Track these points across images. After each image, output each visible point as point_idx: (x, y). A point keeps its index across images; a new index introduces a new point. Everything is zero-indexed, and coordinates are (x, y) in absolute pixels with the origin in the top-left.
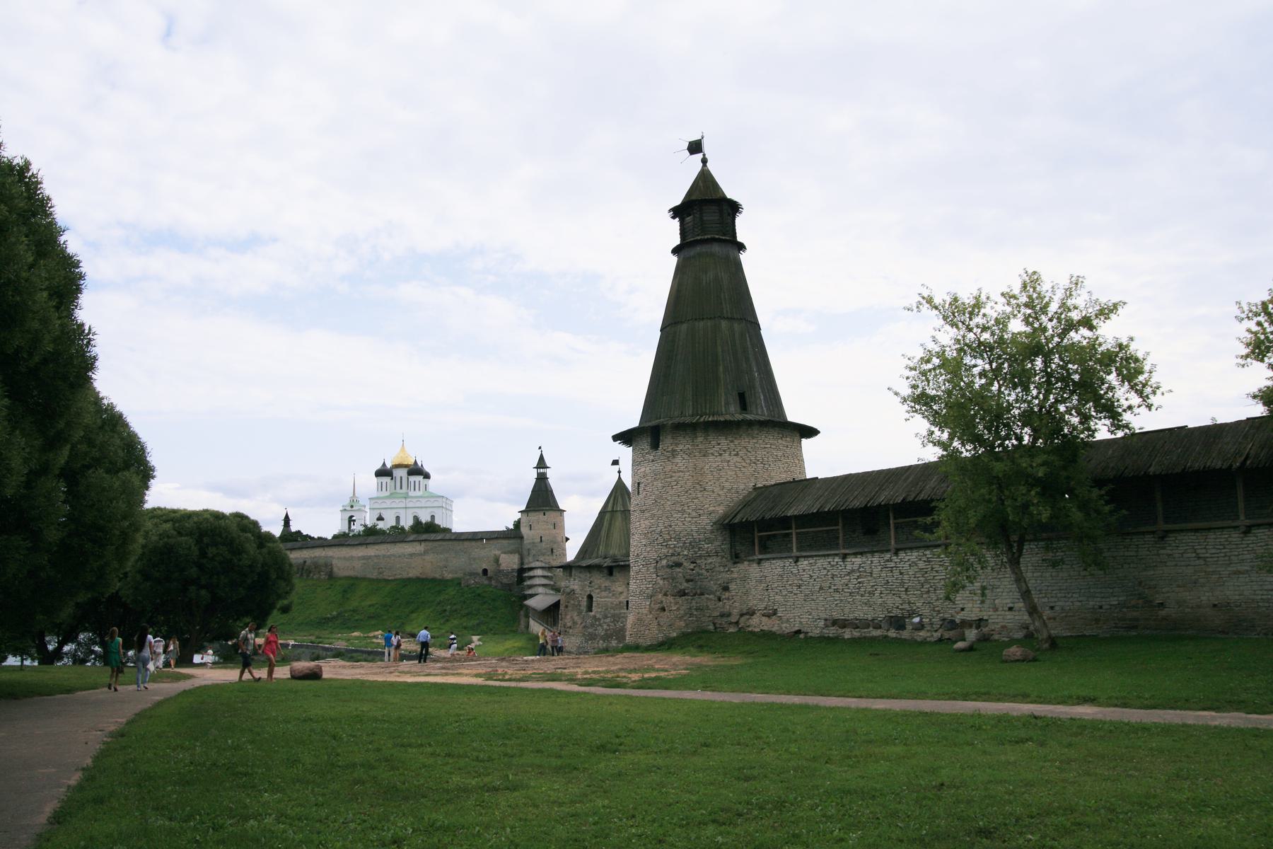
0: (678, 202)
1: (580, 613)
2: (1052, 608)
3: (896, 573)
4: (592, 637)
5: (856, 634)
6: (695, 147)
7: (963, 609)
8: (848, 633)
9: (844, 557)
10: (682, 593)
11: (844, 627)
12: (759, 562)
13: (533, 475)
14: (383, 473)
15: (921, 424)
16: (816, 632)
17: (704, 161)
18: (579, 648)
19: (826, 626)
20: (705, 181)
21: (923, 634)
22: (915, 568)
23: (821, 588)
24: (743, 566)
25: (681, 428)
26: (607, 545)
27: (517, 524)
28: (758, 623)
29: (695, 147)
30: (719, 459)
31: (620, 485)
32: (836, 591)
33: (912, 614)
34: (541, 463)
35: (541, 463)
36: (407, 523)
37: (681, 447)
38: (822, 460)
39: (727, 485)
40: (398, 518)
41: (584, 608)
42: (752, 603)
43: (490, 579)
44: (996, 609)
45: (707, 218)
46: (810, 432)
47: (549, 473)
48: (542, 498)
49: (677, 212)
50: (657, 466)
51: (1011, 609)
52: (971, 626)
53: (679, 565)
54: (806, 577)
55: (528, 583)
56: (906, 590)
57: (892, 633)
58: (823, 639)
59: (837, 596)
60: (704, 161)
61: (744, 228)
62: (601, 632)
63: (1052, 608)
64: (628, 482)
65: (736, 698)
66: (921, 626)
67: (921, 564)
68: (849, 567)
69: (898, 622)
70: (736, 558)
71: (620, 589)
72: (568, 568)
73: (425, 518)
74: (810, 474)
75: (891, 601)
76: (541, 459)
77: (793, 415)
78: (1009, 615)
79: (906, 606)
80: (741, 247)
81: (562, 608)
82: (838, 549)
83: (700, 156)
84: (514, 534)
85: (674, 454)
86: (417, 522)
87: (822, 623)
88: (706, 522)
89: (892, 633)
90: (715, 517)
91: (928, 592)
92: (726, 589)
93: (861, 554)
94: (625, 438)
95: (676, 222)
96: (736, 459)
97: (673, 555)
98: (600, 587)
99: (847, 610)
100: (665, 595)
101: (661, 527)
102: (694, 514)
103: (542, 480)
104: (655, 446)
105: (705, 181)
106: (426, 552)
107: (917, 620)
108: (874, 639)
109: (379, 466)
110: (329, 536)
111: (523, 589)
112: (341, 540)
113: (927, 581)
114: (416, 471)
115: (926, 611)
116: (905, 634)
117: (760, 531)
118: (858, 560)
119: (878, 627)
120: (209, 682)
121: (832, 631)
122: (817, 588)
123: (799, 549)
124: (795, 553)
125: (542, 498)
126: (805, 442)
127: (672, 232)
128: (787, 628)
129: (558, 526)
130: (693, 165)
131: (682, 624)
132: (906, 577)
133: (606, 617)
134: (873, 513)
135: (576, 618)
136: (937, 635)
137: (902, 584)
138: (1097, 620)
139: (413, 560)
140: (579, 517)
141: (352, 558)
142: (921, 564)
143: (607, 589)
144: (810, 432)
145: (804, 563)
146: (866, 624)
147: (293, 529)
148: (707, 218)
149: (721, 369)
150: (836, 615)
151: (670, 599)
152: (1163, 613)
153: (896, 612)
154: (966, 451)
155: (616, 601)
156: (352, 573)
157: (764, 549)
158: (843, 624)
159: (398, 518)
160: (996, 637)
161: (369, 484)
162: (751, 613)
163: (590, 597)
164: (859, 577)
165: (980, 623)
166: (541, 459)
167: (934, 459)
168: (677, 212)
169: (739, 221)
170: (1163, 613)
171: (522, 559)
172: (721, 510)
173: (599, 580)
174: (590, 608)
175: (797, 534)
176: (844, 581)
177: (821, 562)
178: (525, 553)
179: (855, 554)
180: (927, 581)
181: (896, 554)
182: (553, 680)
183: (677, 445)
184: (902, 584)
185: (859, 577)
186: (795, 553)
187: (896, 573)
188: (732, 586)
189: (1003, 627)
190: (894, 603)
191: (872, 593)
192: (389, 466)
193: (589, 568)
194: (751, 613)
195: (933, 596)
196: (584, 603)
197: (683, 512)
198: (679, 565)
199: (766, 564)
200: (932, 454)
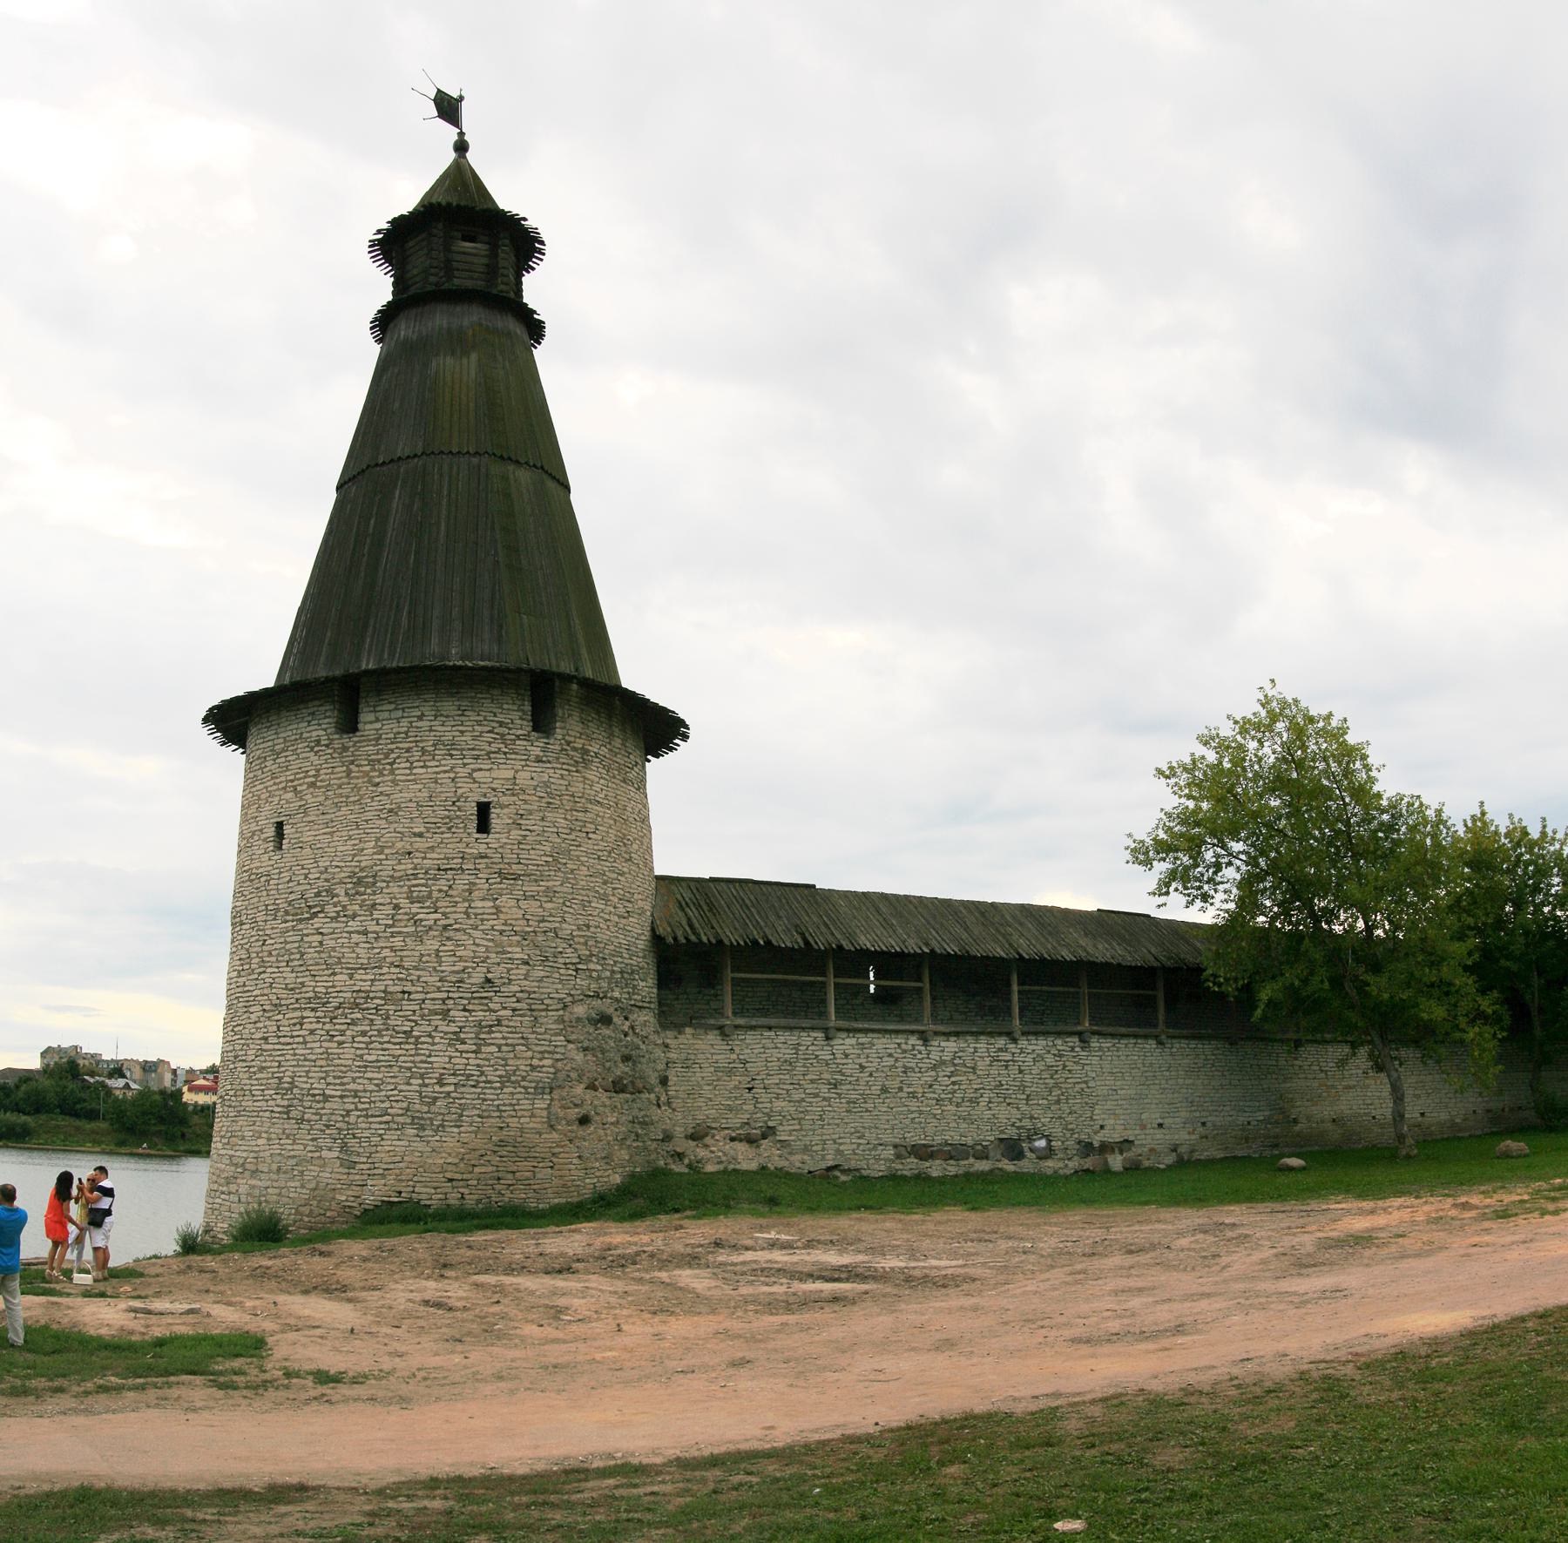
2: (1204, 1124)
3: (1014, 1070)
5: (952, 1169)
7: (1102, 1127)
11: (932, 1156)
16: (878, 1169)
17: (461, 147)
19: (898, 1156)
21: (1050, 1165)
22: (1041, 1065)
23: (884, 1090)
29: (448, 108)
32: (913, 1095)
33: (1032, 1135)
42: (706, 1113)
44: (1143, 1127)
45: (458, 264)
50: (551, 774)
51: (1160, 1125)
52: (1113, 1151)
54: (850, 1068)
56: (1027, 1099)
57: (1008, 1166)
58: (894, 1178)
59: (913, 1105)
60: (461, 147)
63: (1204, 1124)
65: (780, 977)
66: (1049, 1153)
67: (1050, 1060)
68: (935, 1056)
69: (1013, 1148)
75: (1004, 1113)
78: (1159, 1134)
79: (1027, 1123)
82: (917, 1021)
85: (585, 759)
87: (889, 1153)
89: (1008, 1166)
91: (1058, 1102)
93: (957, 1034)
99: (930, 1130)
100: (592, 1087)
107: (1042, 1143)
108: (981, 1176)
113: (1057, 1085)
115: (1057, 1130)
116: (1027, 1165)
117: (735, 969)
118: (951, 1045)
119: (983, 1155)
120: (1261, 1207)
121: (911, 1165)
122: (876, 1089)
123: (1093, 1020)
124: (832, 1020)
131: (624, 1154)
132: (1028, 1078)
136: (1074, 1164)
137: (1022, 1088)
138: (1247, 1140)
142: (1050, 1060)
145: (845, 1043)
146: (954, 1153)
148: (458, 264)
150: (914, 1138)
151: (602, 1096)
152: (1297, 1128)
153: (1012, 1133)
158: (923, 1152)
160: (1146, 1164)
164: (952, 1074)
165: (1126, 1144)
170: (1297, 1128)
176: (928, 1077)
177: (882, 1043)
179: (947, 1035)
180: (1057, 1085)
184: (1022, 1088)
185: (952, 1074)
186: (832, 1020)
187: (1014, 1070)
189: (1152, 1150)
190: (1004, 1118)
191: (974, 1101)
195: (1065, 1107)
198: (605, 1020)
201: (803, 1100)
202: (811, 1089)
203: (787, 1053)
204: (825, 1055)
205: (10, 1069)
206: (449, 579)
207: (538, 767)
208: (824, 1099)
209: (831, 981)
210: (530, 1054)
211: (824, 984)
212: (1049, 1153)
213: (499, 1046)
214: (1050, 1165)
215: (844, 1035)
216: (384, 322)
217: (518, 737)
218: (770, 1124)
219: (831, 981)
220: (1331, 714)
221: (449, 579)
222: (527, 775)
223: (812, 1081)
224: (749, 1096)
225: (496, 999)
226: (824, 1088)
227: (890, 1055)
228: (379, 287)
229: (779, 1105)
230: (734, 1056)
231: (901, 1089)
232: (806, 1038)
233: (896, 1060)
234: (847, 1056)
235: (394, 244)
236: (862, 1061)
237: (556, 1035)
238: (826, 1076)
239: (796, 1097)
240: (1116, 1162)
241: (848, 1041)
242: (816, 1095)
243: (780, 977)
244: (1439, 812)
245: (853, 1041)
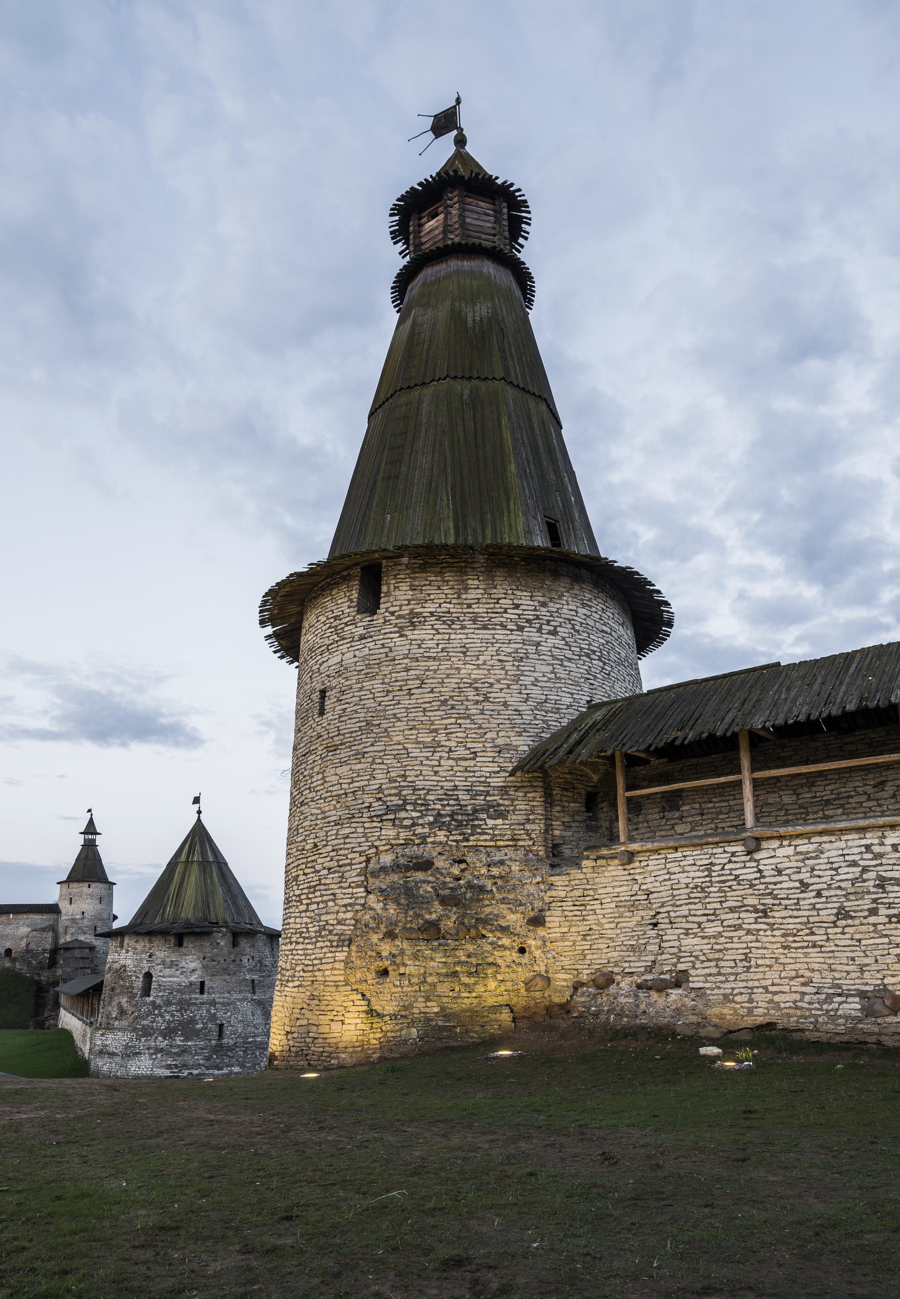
1: (132, 996)
4: (147, 1032)
13: (81, 840)
18: (127, 1047)
23: (843, 914)
25: (431, 559)
26: (176, 906)
30: (516, 636)
34: (91, 829)
35: (91, 829)
37: (431, 607)
39: (536, 692)
43: (14, 960)
47: (99, 840)
48: (89, 868)
53: (426, 865)
65: (722, 779)
71: (192, 965)
76: (91, 822)
81: (106, 991)
87: (853, 1006)
96: (552, 641)
97: (407, 843)
98: (163, 963)
100: (390, 935)
101: (381, 778)
102: (462, 752)
104: (370, 603)
117: (629, 788)
122: (827, 915)
125: (89, 868)
133: (168, 1003)
135: (125, 1005)
143: (173, 964)
145: (777, 854)
148: (462, 230)
149: (513, 467)
155: (183, 980)
163: (148, 976)
166: (91, 822)
173: (162, 951)
174: (146, 991)
175: (757, 784)
178: (61, 930)
183: (423, 602)
188: (553, 919)
193: (150, 934)
196: (139, 983)
197: (435, 746)
198: (426, 865)
201: (720, 934)
202: (731, 918)
203: (697, 875)
204: (749, 873)
206: (464, 463)
207: (358, 645)
208: (749, 932)
209: (746, 777)
210: (337, 908)
211: (739, 784)
213: (318, 903)
215: (775, 844)
216: (403, 282)
217: (346, 624)
218: (681, 967)
219: (746, 777)
221: (464, 463)
222: (351, 654)
223: (732, 910)
224: (653, 933)
225: (320, 861)
226: (749, 918)
227: (854, 864)
228: (393, 258)
229: (689, 942)
230: (636, 887)
231: (873, 912)
232: (720, 855)
233: (865, 870)
234: (780, 872)
235: (412, 208)
236: (805, 876)
237: (358, 886)
238: (751, 901)
239: (710, 931)
241: (781, 852)
242: (738, 927)
245: (790, 851)
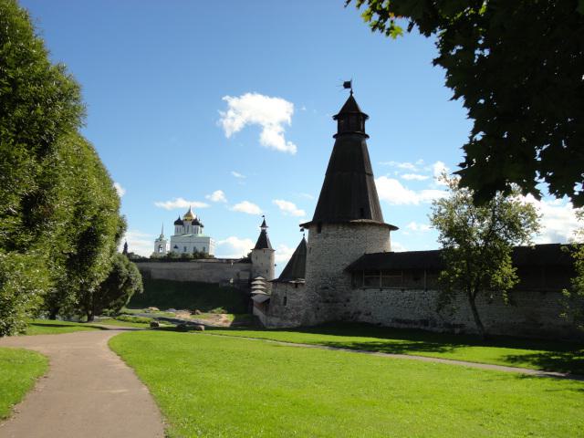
0: (337, 113)
5: (406, 326)
6: (347, 85)
8: (402, 326)
9: (403, 290)
10: (327, 301)
12: (364, 289)
14: (178, 222)
15: (438, 233)
17: (351, 92)
20: (351, 105)
24: (358, 291)
27: (250, 255)
28: (362, 318)
31: (303, 241)
34: (264, 224)
35: (264, 224)
36: (190, 252)
38: (398, 244)
40: (185, 248)
41: (282, 303)
46: (394, 228)
47: (268, 230)
49: (336, 117)
53: (327, 288)
55: (255, 287)
60: (351, 92)
61: (369, 127)
62: (290, 316)
64: (307, 240)
65: (360, 221)
69: (425, 322)
70: (354, 287)
72: (275, 282)
73: (200, 250)
74: (392, 250)
77: (387, 220)
80: (367, 136)
83: (349, 90)
84: (247, 260)
85: (327, 235)
86: (195, 253)
88: (341, 269)
90: (344, 267)
92: (348, 301)
94: (305, 226)
95: (336, 122)
103: (263, 235)
104: (319, 231)
105: (351, 105)
106: (201, 268)
109: (176, 219)
110: (148, 256)
111: (252, 285)
112: (152, 259)
114: (196, 223)
116: (427, 328)
118: (409, 292)
119: (416, 324)
121: (395, 325)
125: (263, 243)
126: (392, 233)
127: (333, 127)
128: (375, 321)
129: (270, 258)
130: (345, 95)
134: (417, 266)
136: (441, 330)
139: (190, 272)
140: (282, 256)
141: (161, 269)
144: (394, 228)
145: (385, 292)
146: (406, 322)
147: (129, 251)
150: (398, 317)
151: (322, 304)
154: (456, 247)
156: (161, 277)
157: (367, 283)
159: (185, 248)
161: (170, 231)
162: (359, 313)
163: (285, 298)
165: (461, 326)
167: (436, 248)
168: (336, 117)
169: (367, 123)
171: (251, 275)
172: (348, 263)
174: (285, 303)
181: (426, 290)
182: (521, 357)
192: (182, 219)
194: (359, 313)
196: (282, 300)
198: (327, 288)
199: (368, 291)
200: (438, 246)
205: (271, 96)
212: (435, 325)
214: (435, 329)
220: (374, 28)
240: (457, 331)
243: (386, 341)
244: (456, 97)
